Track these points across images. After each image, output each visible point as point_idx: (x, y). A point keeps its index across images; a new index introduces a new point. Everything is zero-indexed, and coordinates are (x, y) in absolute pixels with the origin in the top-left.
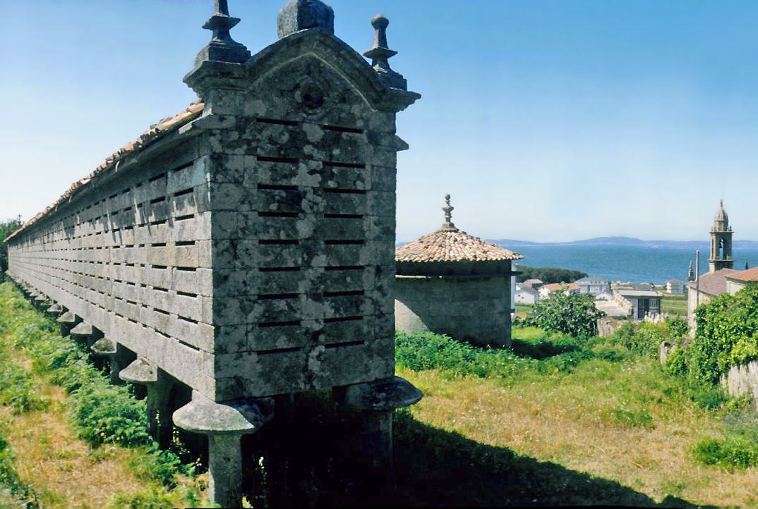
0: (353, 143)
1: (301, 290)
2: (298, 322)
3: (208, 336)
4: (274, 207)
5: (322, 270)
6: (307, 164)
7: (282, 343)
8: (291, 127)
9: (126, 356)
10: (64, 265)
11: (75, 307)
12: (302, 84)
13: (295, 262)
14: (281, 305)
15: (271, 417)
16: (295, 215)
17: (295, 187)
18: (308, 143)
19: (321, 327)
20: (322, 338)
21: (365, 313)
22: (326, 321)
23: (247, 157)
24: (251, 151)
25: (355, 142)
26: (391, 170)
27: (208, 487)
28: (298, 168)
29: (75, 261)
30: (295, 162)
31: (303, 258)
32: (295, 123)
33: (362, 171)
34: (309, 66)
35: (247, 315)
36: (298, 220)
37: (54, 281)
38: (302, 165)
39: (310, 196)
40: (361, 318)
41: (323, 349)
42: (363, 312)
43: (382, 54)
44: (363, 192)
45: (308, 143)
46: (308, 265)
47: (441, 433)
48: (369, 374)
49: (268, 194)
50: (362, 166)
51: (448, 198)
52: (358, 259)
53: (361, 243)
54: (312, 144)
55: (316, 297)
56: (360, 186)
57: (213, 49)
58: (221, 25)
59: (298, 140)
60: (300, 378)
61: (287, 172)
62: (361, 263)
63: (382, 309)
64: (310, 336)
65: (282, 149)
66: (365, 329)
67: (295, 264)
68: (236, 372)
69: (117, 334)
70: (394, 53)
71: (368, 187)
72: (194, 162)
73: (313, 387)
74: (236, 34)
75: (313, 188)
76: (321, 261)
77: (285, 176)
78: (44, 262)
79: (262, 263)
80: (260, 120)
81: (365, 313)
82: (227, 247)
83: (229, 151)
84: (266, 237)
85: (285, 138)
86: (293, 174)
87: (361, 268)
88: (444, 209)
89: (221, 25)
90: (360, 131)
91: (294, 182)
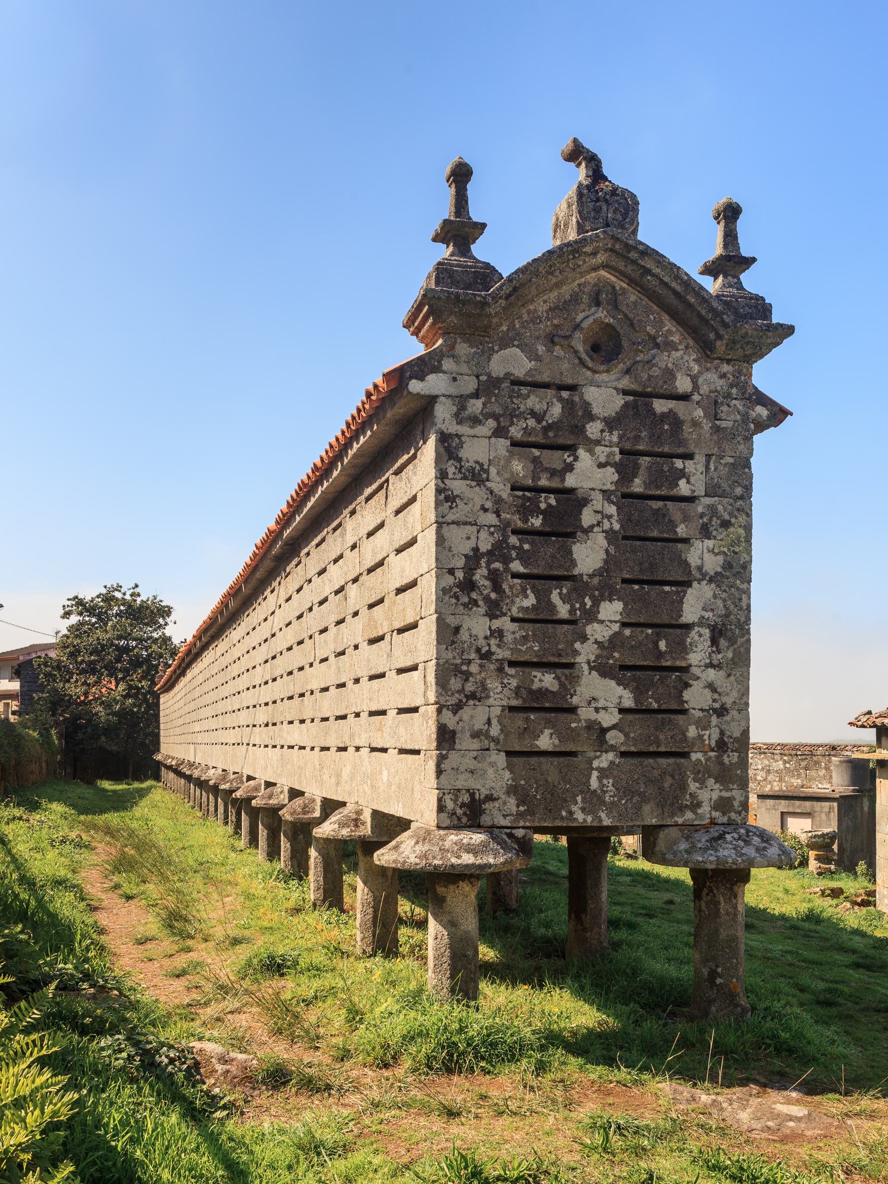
2: (573, 710)
3: (430, 721)
4: (537, 522)
6: (591, 452)
7: (545, 742)
8: (565, 394)
12: (585, 325)
14: (547, 680)
15: (712, 285)
16: (572, 535)
17: (572, 491)
22: (622, 711)
23: (493, 440)
26: (735, 485)
27: (76, 597)
28: (576, 459)
30: (571, 448)
32: (572, 388)
33: (689, 464)
34: (598, 293)
36: (575, 543)
38: (581, 452)
39: (598, 501)
40: (684, 712)
43: (732, 263)
44: (691, 499)
48: (699, 811)
49: (535, 460)
50: (689, 456)
56: (684, 488)
57: (442, 271)
58: (460, 231)
59: (578, 415)
70: (751, 261)
71: (700, 491)
74: (482, 250)
75: (604, 492)
80: (517, 382)
82: (464, 585)
85: (557, 410)
86: (570, 468)
87: (688, 627)
89: (460, 231)
91: (570, 481)
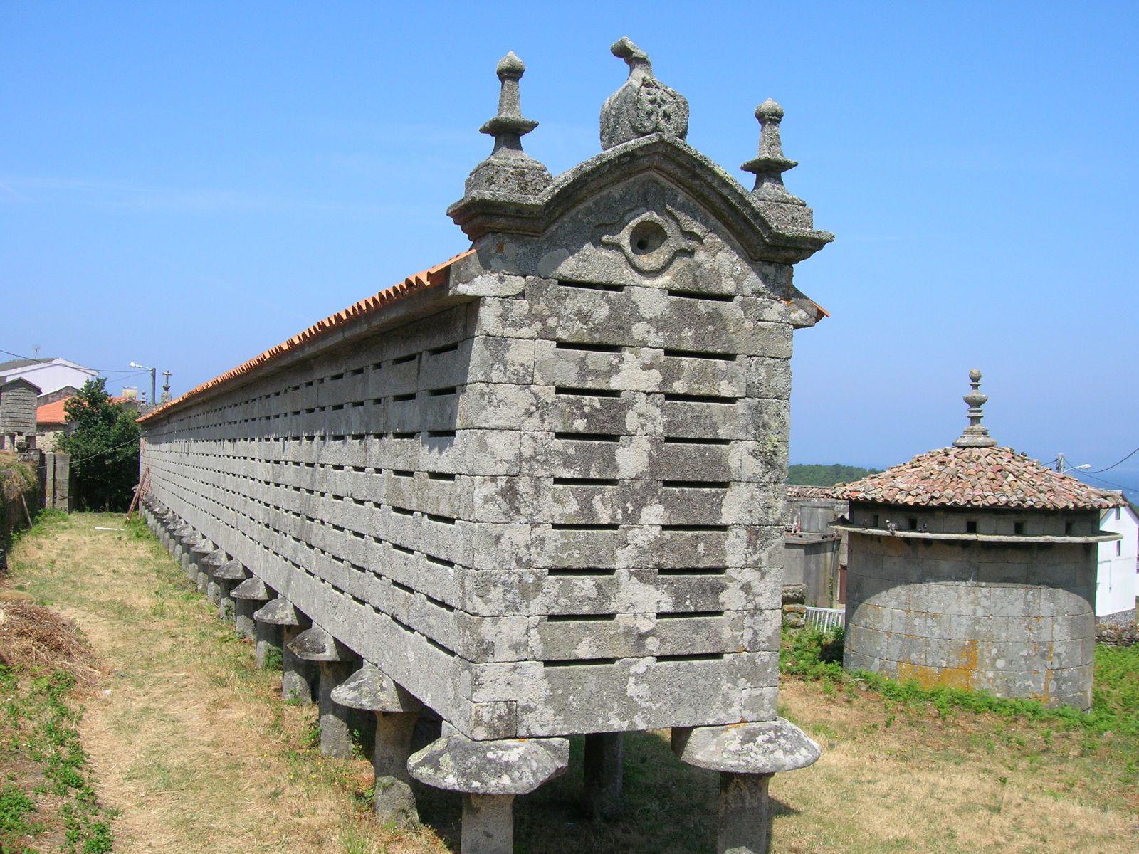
0: (714, 317)
1: (620, 564)
5: (657, 531)
9: (349, 663)
10: (246, 486)
11: (267, 570)
13: (613, 517)
14: (586, 584)
18: (642, 319)
19: (652, 626)
20: (652, 644)
21: (726, 607)
22: (661, 615)
24: (546, 334)
25: (720, 316)
29: (268, 483)
31: (625, 510)
35: (529, 601)
37: (229, 515)
39: (642, 404)
41: (650, 661)
42: (723, 604)
45: (642, 319)
46: (633, 519)
47: (593, 734)
51: (975, 379)
52: (719, 513)
53: (725, 485)
54: (650, 321)
55: (640, 574)
60: (612, 709)
61: (604, 369)
62: (725, 520)
63: (758, 599)
64: (632, 641)
65: (597, 330)
66: (727, 633)
67: (613, 519)
68: (509, 695)
69: (334, 626)
72: (459, 345)
73: (632, 724)
76: (654, 514)
77: (597, 374)
78: (204, 475)
79: (557, 516)
81: (726, 607)
83: (509, 331)
84: (567, 474)
85: (603, 312)
86: (614, 370)
87: (724, 528)
88: (967, 401)
90: (728, 298)
91: (614, 384)
